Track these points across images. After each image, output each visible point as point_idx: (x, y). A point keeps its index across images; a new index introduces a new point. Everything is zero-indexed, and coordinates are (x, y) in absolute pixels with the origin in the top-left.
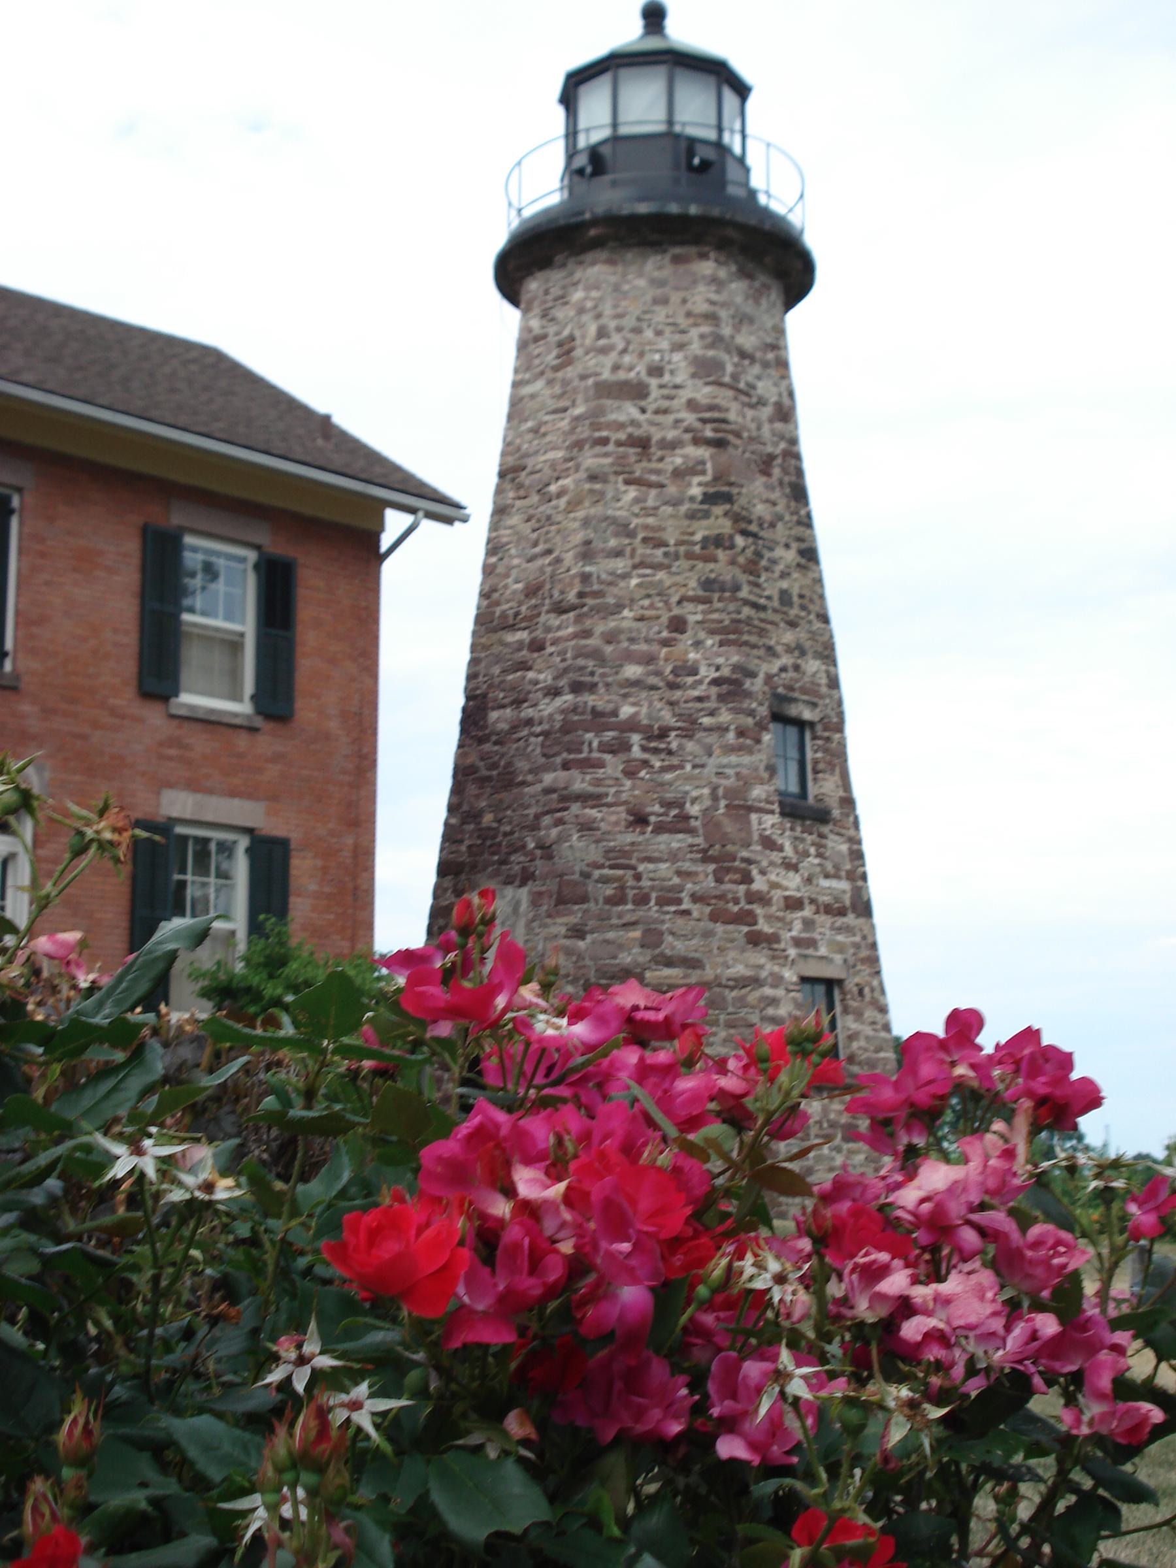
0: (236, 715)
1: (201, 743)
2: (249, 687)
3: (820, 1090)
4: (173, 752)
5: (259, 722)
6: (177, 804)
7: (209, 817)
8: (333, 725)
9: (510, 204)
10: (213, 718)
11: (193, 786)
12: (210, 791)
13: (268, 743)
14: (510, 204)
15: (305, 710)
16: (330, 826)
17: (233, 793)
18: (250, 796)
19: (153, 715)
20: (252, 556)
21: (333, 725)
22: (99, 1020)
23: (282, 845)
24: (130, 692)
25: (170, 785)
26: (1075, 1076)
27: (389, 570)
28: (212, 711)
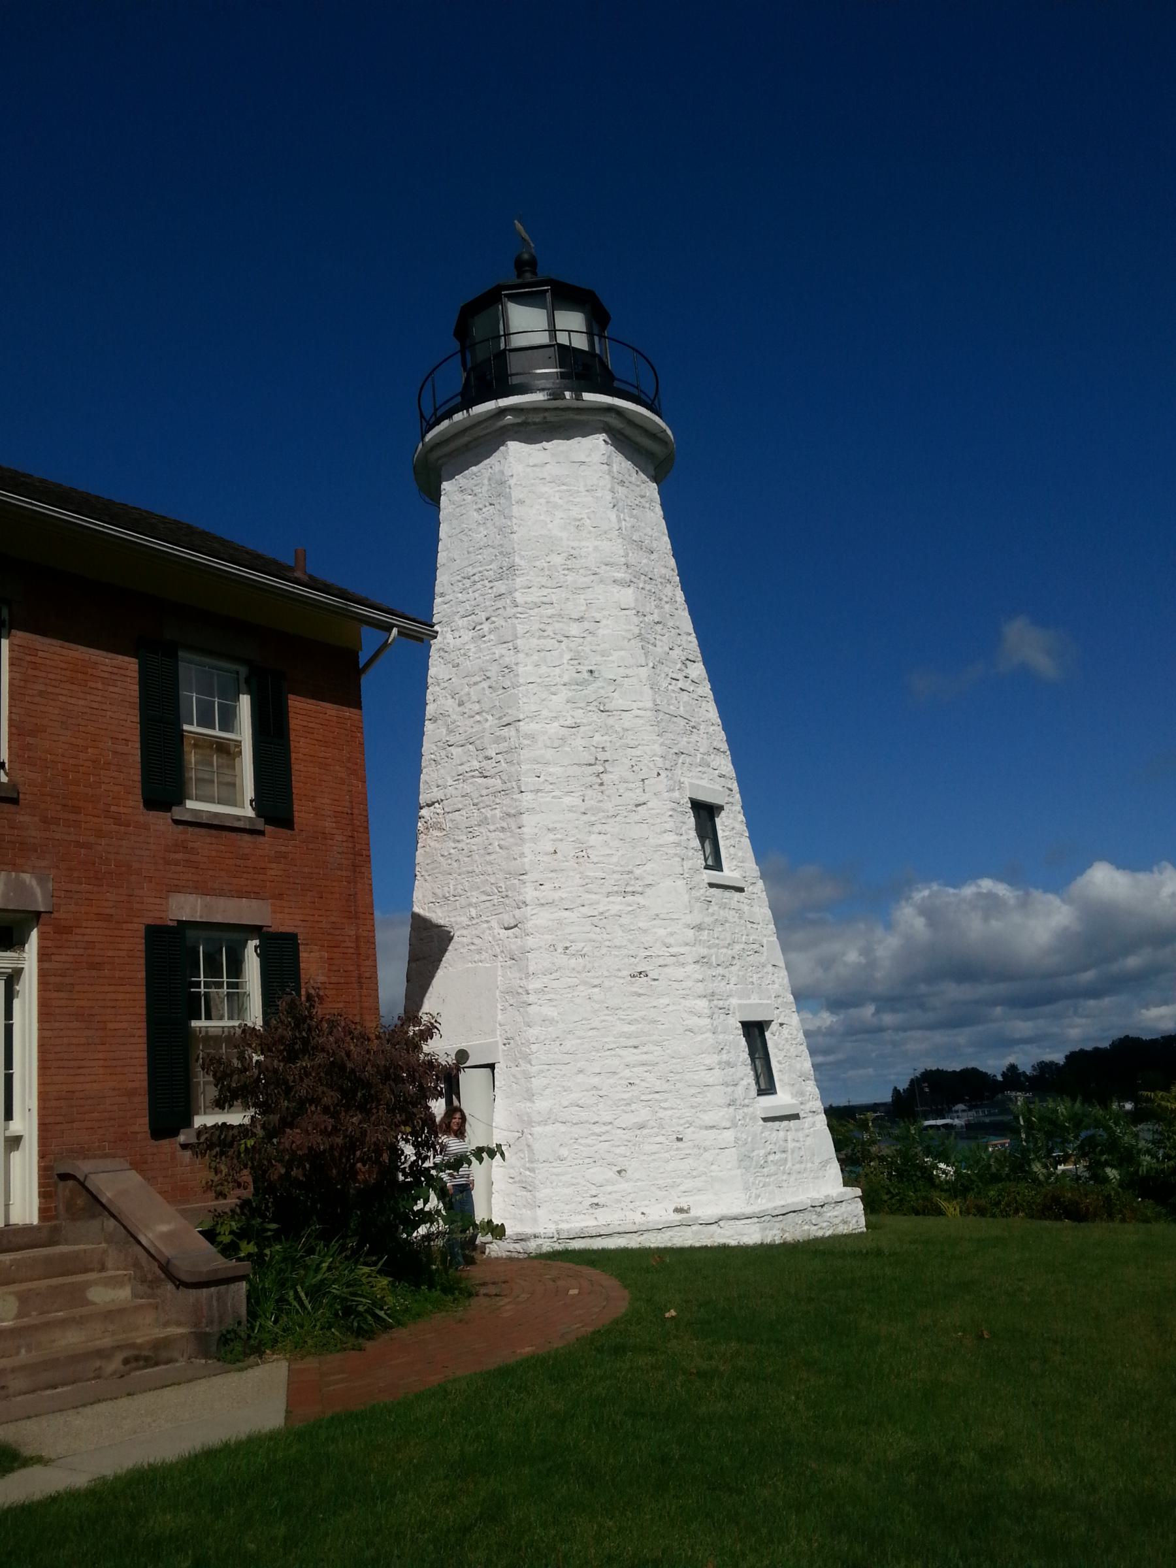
0: (238, 818)
1: (203, 842)
2: (249, 792)
3: (392, 1193)
4: (179, 856)
5: (260, 825)
6: (187, 908)
7: (218, 919)
8: (329, 825)
9: (422, 416)
10: (216, 822)
11: (201, 889)
12: (221, 894)
13: (273, 841)
14: (422, 416)
15: (301, 812)
16: (333, 919)
17: (240, 894)
18: (256, 895)
19: (160, 821)
20: (243, 670)
21: (329, 825)
22: (283, 1171)
23: (290, 940)
24: (136, 799)
25: (178, 889)
26: (1000, 1078)
27: (364, 680)
28: (216, 815)
